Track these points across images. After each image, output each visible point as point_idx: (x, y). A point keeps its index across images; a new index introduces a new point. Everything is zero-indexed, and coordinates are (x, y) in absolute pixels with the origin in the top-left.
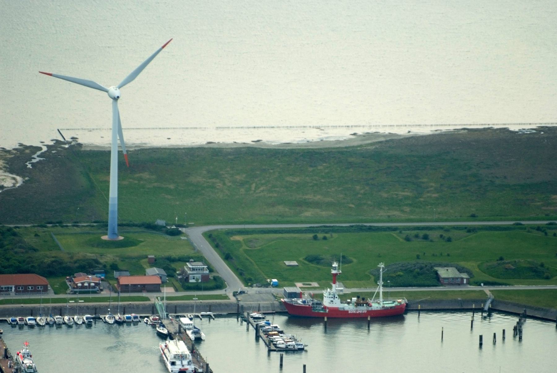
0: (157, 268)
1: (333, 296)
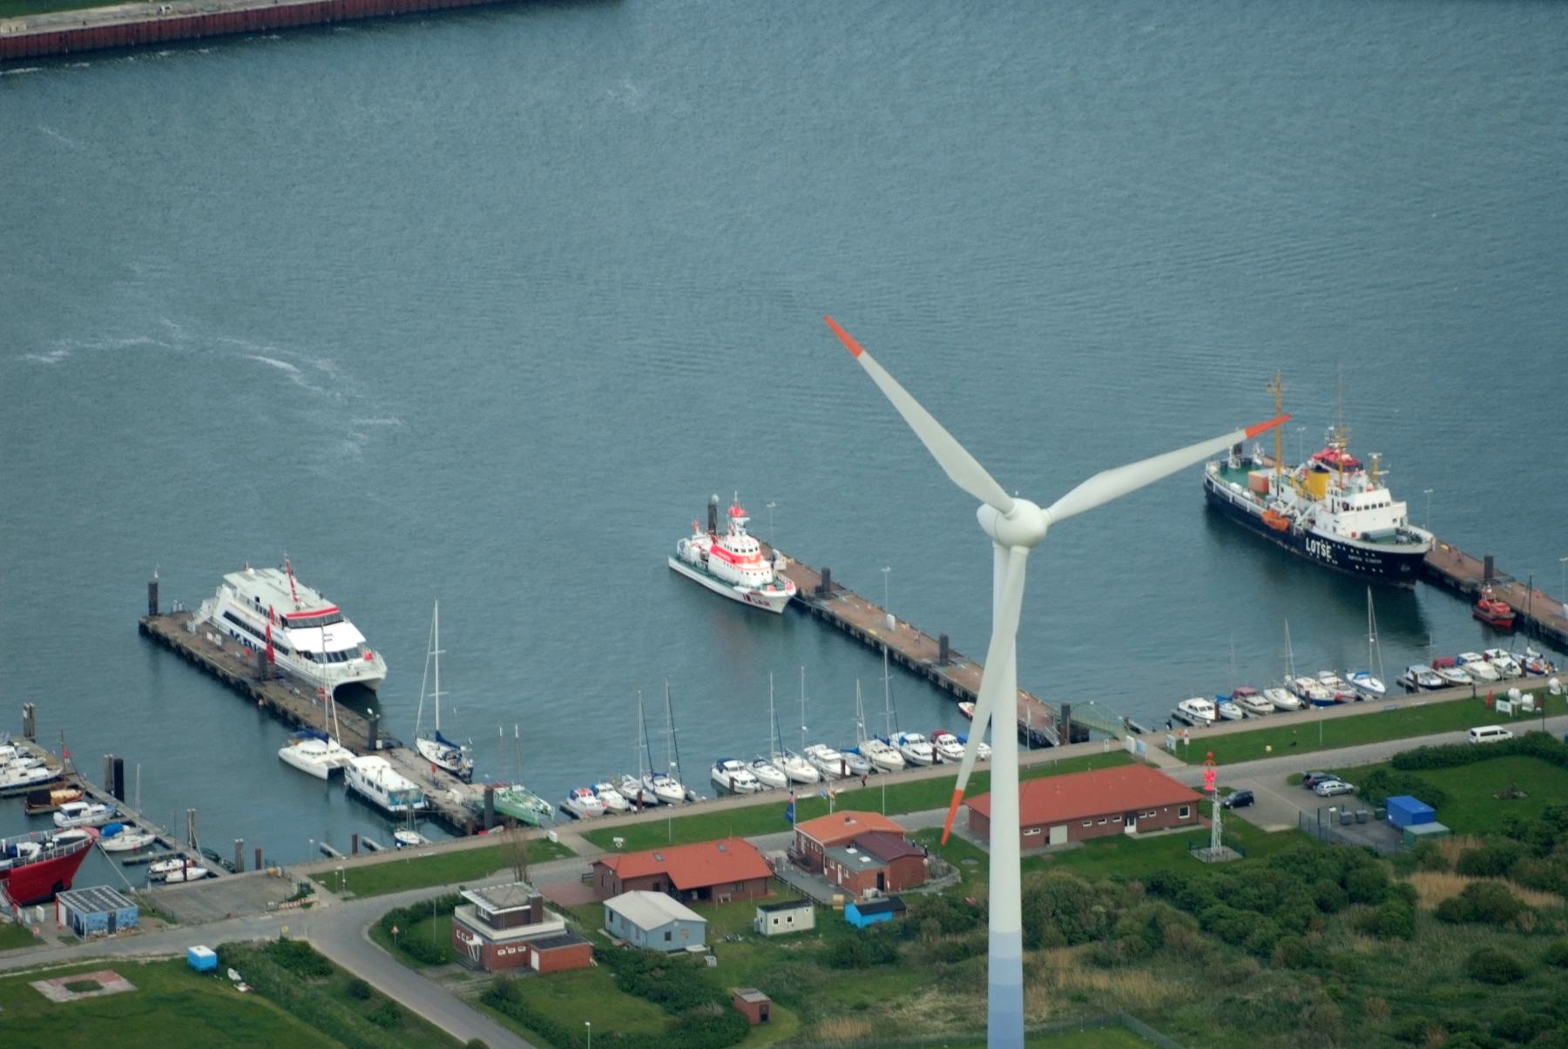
0: (52, 981)
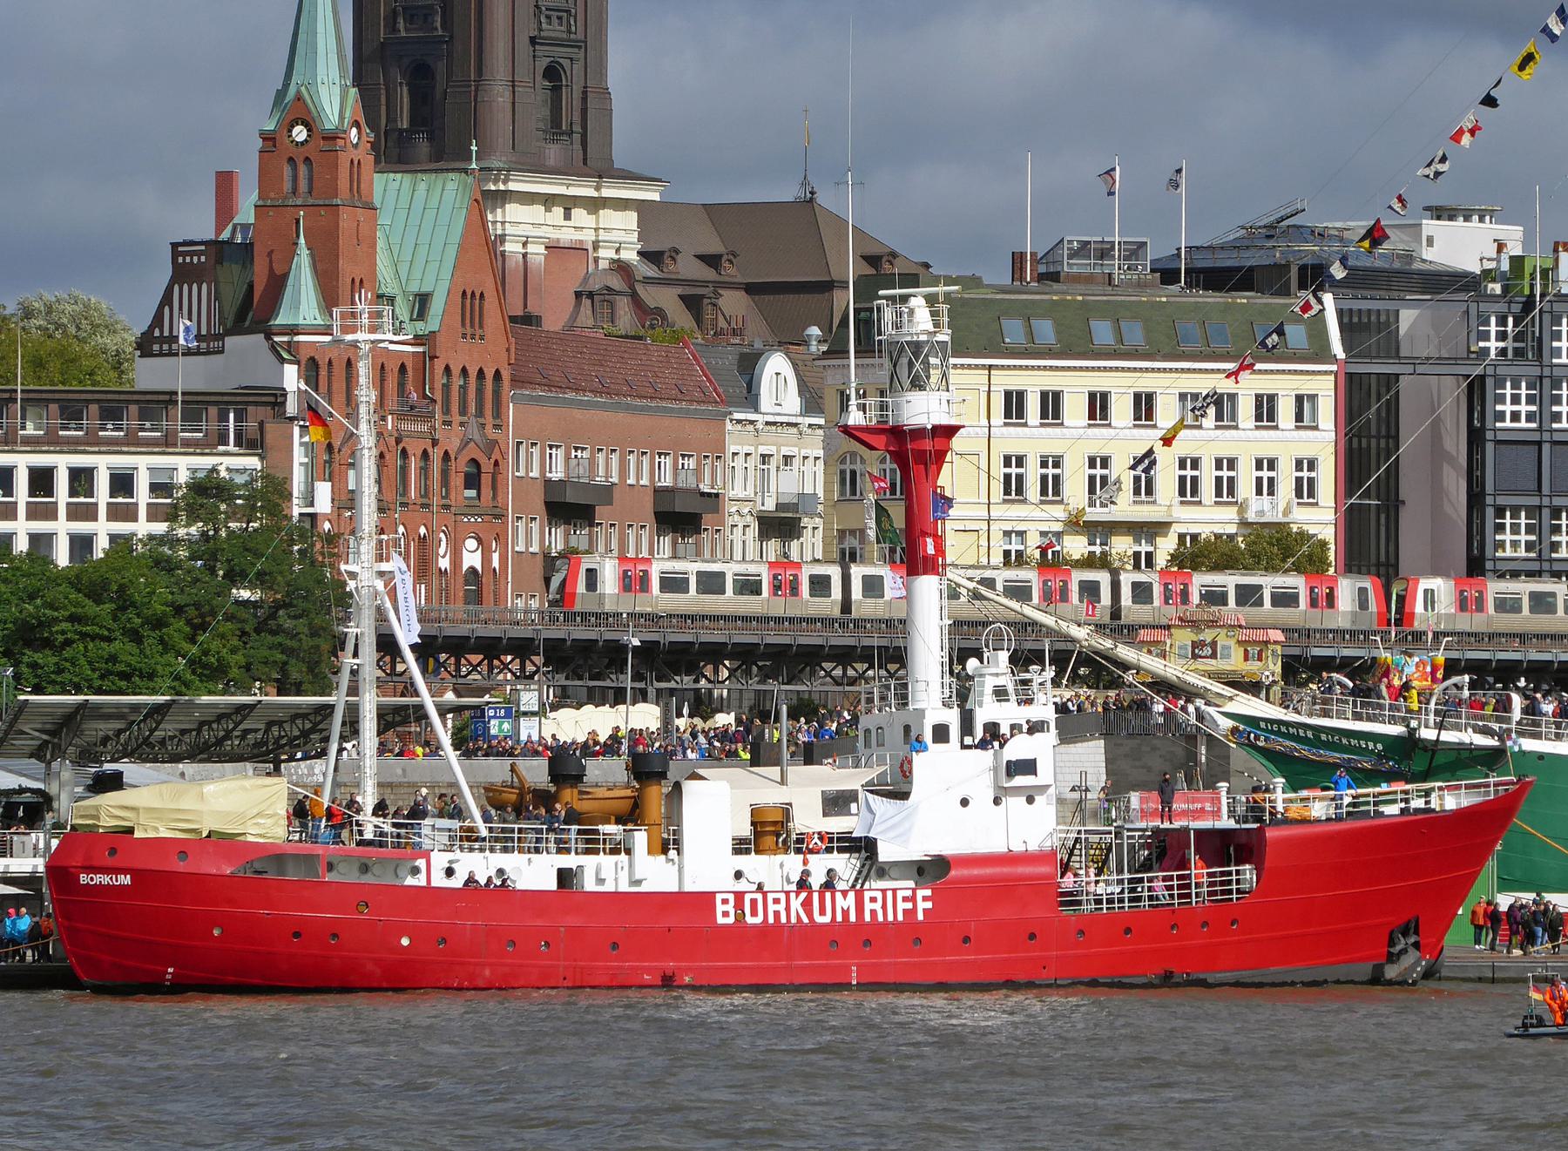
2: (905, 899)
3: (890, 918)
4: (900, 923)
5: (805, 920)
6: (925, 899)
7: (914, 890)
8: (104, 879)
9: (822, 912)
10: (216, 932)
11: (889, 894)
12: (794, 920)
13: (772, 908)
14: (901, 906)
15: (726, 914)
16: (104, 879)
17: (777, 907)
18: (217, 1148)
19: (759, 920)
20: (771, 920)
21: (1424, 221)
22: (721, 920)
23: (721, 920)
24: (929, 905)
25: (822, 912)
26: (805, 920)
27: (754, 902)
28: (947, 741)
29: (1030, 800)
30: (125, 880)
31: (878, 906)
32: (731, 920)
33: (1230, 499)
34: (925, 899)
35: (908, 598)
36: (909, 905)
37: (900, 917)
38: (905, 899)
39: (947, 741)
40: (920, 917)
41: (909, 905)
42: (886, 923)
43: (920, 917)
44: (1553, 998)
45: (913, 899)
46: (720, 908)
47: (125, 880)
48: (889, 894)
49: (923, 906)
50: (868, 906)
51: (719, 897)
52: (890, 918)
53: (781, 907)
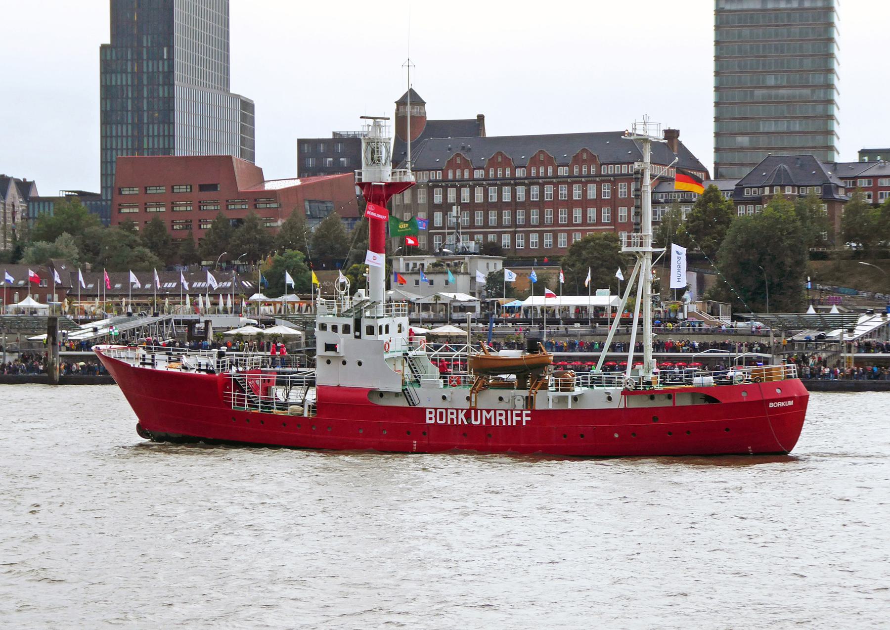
1: (350, 322)
2: (517, 415)
3: (509, 424)
4: (514, 427)
5: (466, 423)
6: (527, 415)
7: (522, 411)
8: (782, 404)
9: (476, 420)
10: (616, 436)
11: (509, 412)
12: (460, 423)
13: (450, 416)
14: (515, 419)
15: (431, 419)
16: (782, 404)
17: (452, 416)
18: (808, 626)
19: (478, 423)
20: (449, 422)
21: (298, 183)
22: (428, 421)
23: (428, 421)
24: (529, 419)
25: (476, 420)
26: (466, 423)
27: (441, 413)
28: (349, 333)
29: (329, 362)
30: (791, 403)
31: (503, 418)
32: (433, 421)
33: (408, 262)
34: (527, 415)
35: (456, 281)
36: (519, 418)
37: (514, 424)
38: (517, 415)
39: (349, 333)
40: (524, 424)
41: (519, 418)
42: (507, 426)
43: (524, 424)
44: (129, 449)
45: (520, 415)
46: (428, 416)
47: (791, 403)
48: (509, 412)
49: (525, 419)
50: (498, 418)
51: (428, 411)
52: (509, 424)
53: (454, 417)
